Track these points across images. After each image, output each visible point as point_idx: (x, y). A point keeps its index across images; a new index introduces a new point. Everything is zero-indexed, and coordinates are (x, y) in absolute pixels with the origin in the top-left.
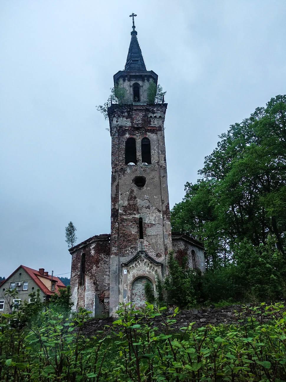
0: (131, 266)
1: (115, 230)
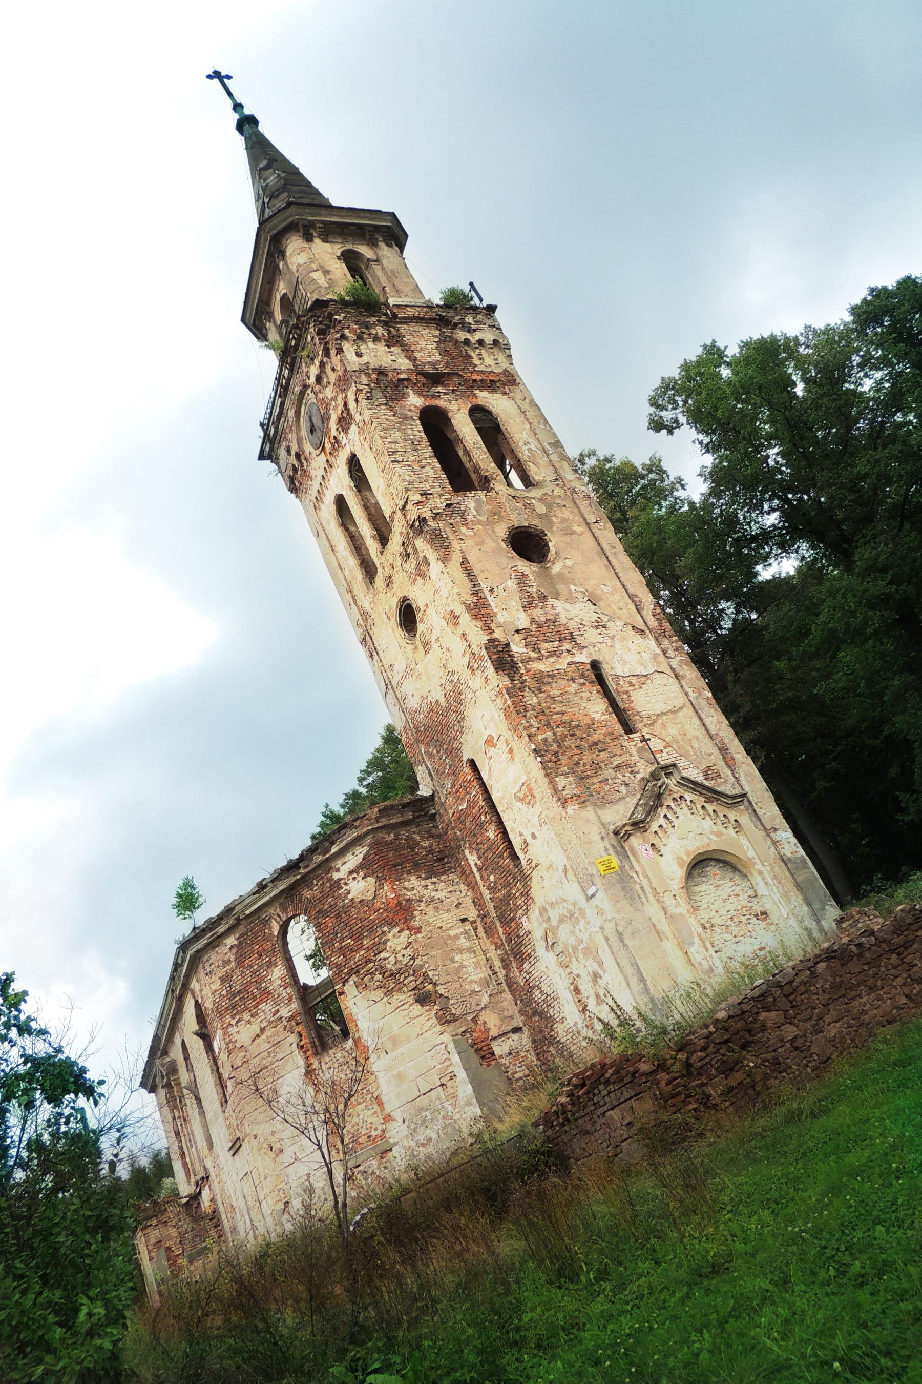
0: (654, 826)
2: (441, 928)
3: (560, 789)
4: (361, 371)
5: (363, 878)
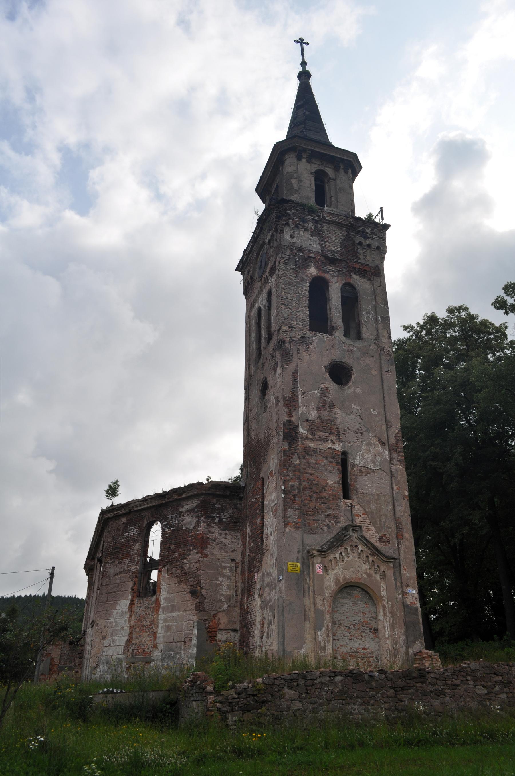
0: (331, 557)
1: (294, 471)
2: (219, 559)
3: (288, 516)
4: (288, 246)
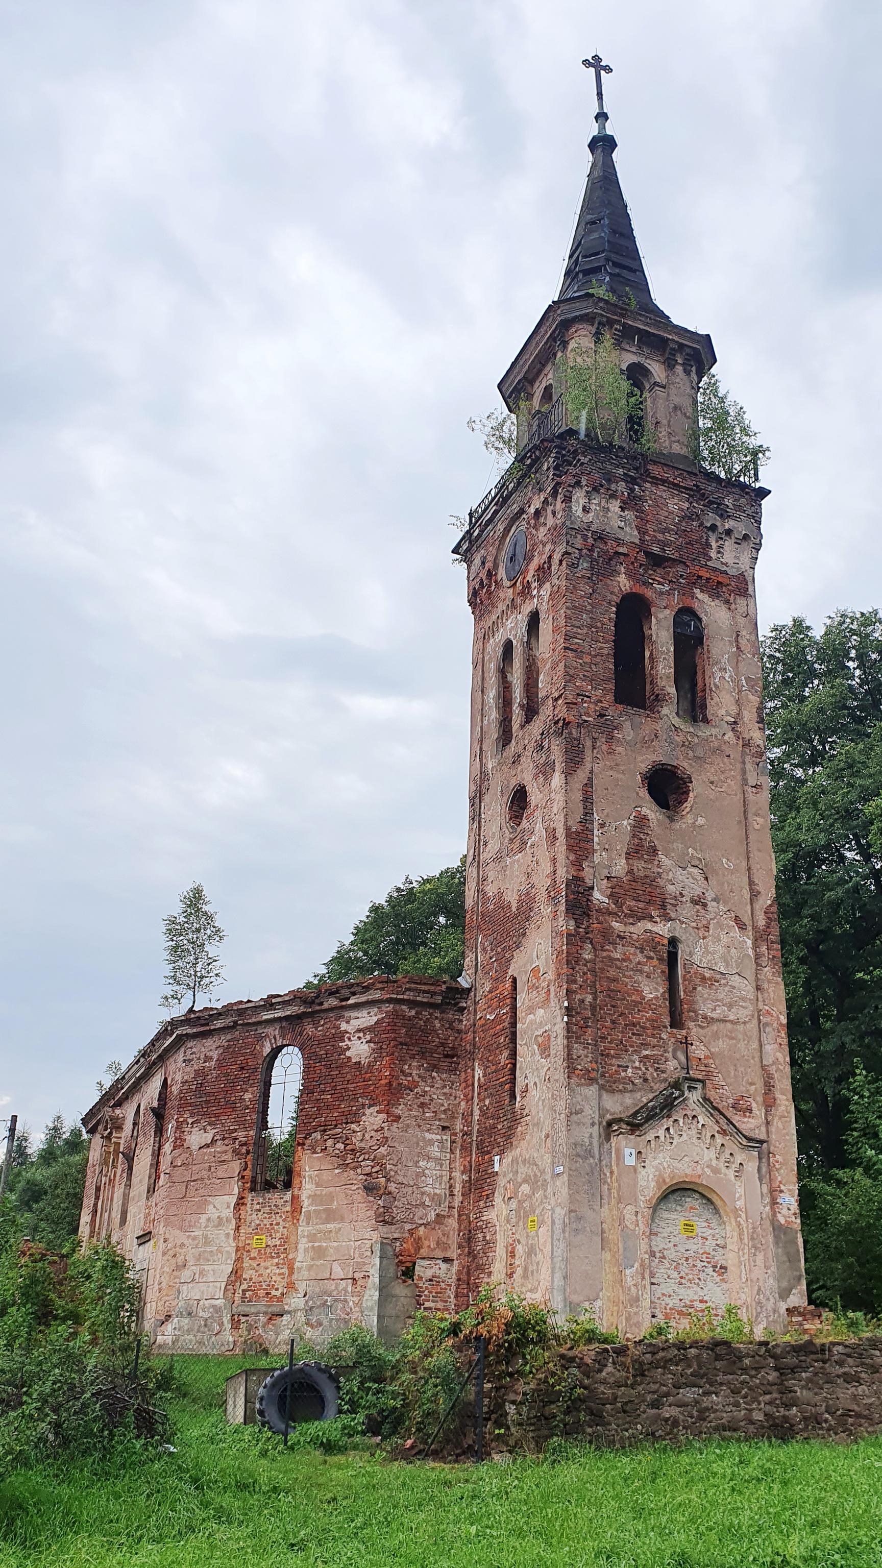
0: (651, 1136)
5: (367, 1042)
